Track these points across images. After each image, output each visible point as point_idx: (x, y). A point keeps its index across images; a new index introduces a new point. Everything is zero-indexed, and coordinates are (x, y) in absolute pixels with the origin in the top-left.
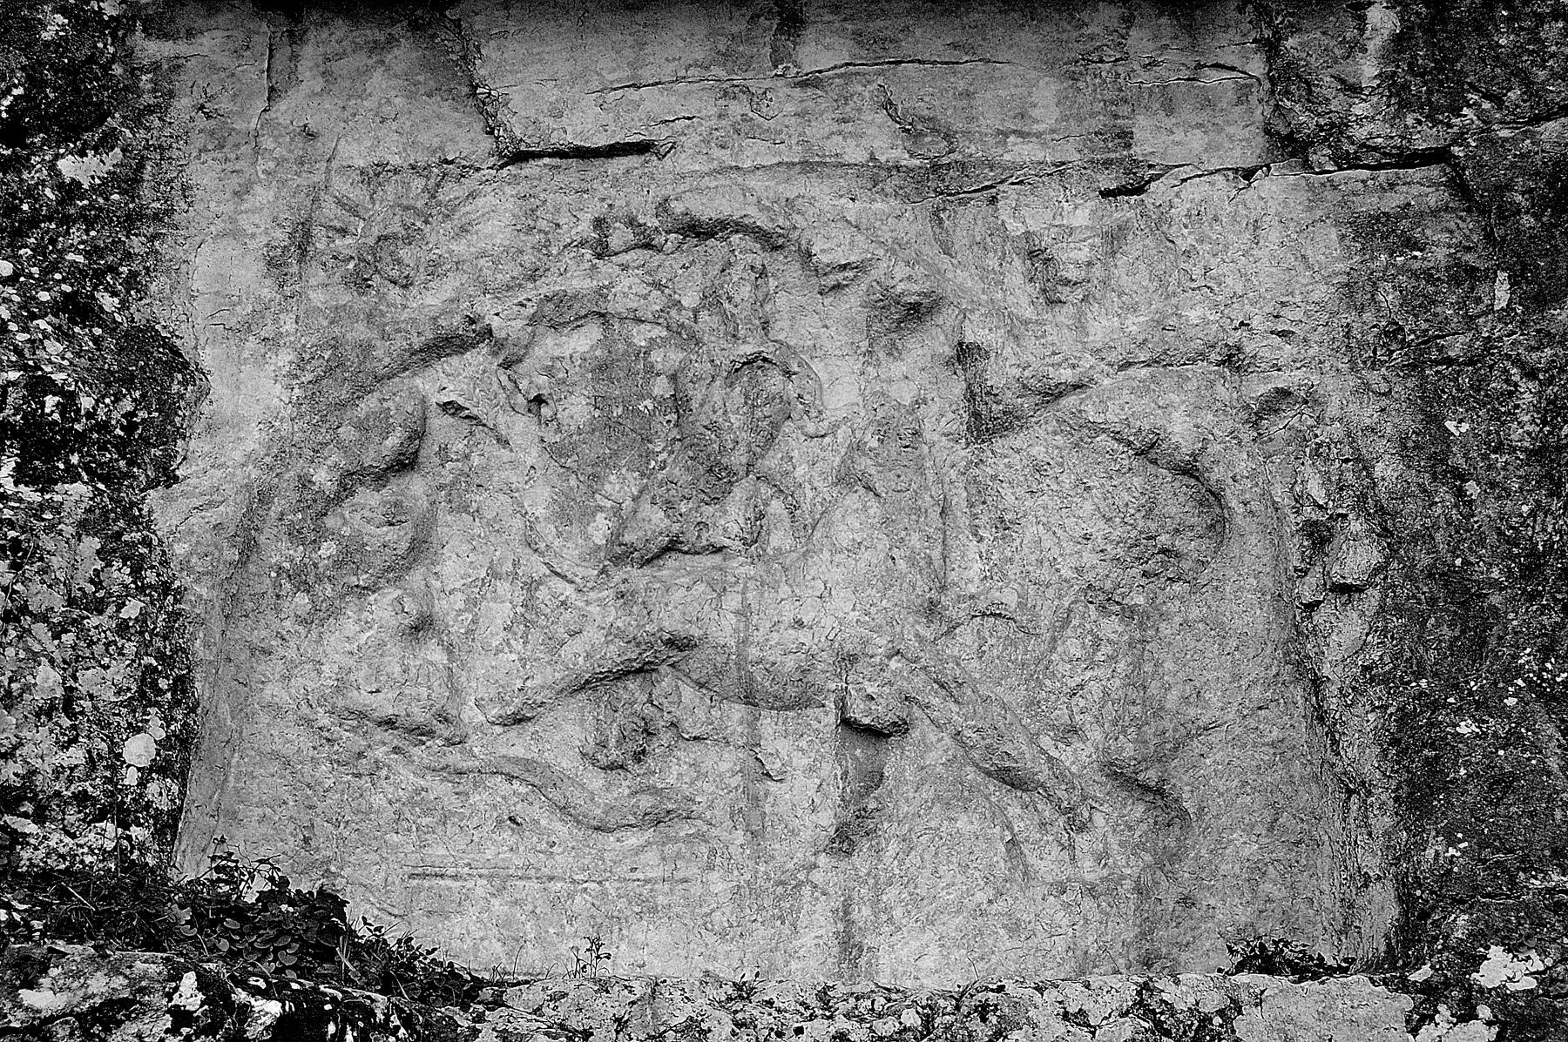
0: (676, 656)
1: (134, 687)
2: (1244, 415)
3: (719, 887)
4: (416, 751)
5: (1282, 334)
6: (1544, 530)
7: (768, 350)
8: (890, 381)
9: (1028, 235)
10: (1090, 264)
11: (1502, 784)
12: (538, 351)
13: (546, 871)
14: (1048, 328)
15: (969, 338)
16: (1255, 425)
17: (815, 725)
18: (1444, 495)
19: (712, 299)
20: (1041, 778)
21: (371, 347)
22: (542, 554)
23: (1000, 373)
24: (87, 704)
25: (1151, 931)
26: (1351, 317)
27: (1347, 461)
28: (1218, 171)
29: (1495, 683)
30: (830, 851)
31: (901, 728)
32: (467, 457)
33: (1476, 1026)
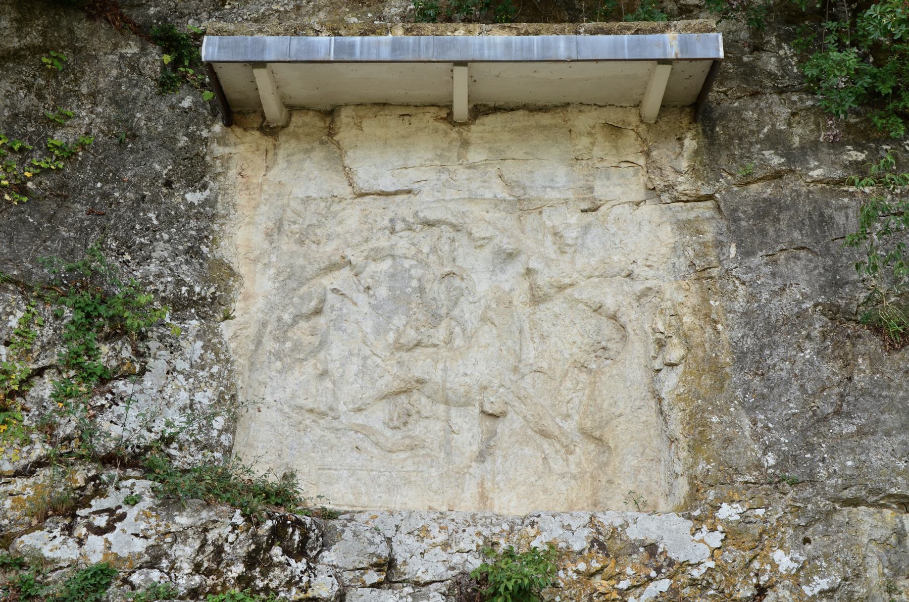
0: (419, 386)
3: (435, 474)
4: (322, 422)
5: (649, 266)
7: (455, 270)
8: (501, 282)
9: (554, 227)
10: (577, 238)
11: (728, 440)
12: (368, 269)
13: (370, 468)
15: (531, 266)
16: (638, 301)
18: (709, 329)
19: (434, 250)
20: (556, 434)
21: (305, 267)
23: (542, 280)
24: (198, 406)
26: (675, 260)
30: (476, 461)
31: (504, 414)
33: (717, 533)
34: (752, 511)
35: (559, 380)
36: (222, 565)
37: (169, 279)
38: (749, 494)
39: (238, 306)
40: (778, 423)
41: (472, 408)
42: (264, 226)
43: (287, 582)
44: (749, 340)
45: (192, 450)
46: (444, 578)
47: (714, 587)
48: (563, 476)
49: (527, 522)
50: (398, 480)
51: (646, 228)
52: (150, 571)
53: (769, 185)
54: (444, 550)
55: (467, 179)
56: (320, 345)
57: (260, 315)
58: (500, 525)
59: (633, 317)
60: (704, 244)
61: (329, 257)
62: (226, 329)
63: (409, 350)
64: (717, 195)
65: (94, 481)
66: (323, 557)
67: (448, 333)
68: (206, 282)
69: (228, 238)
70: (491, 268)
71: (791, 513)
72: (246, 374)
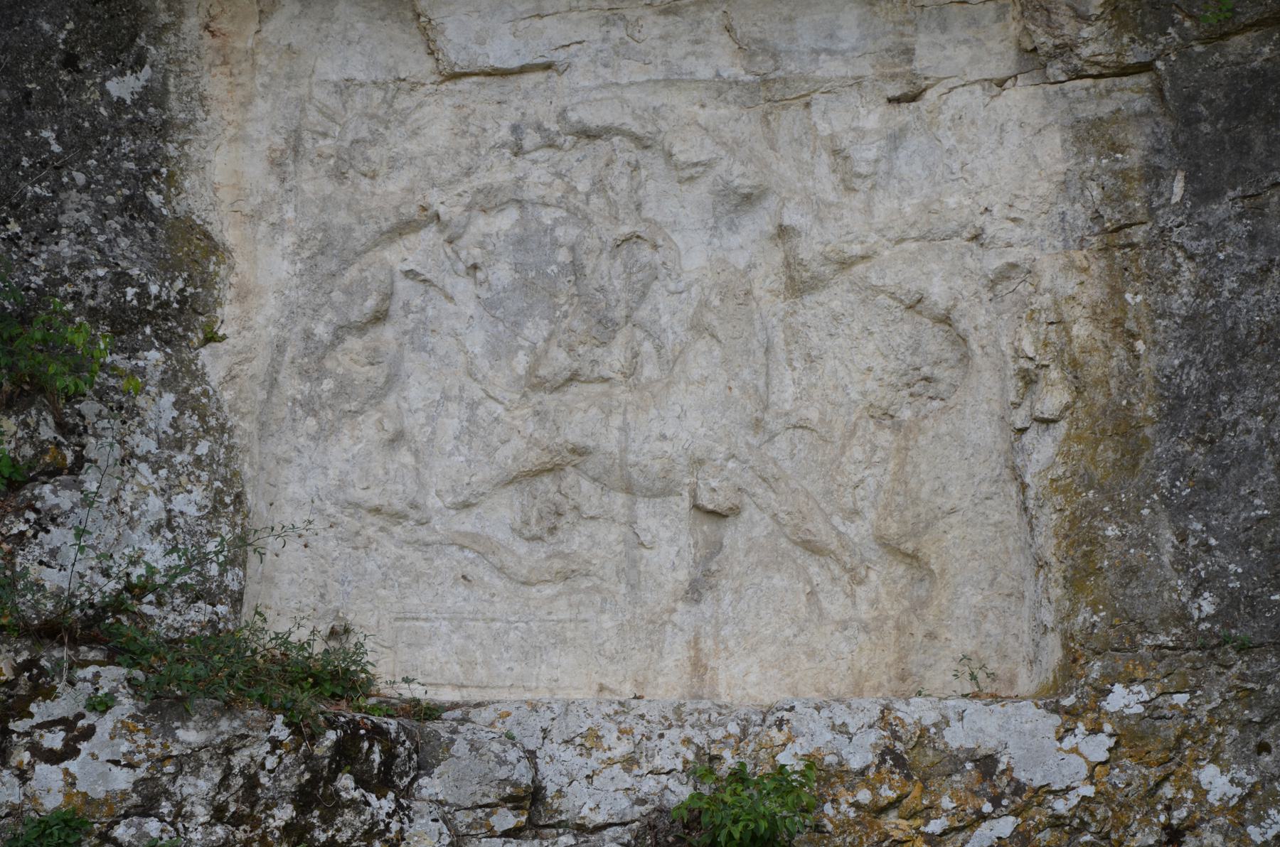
0: (577, 460)
1: (210, 505)
2: (984, 281)
3: (608, 624)
4: (397, 530)
5: (1014, 220)
6: (1188, 379)
7: (641, 229)
8: (730, 250)
9: (832, 137)
10: (877, 161)
11: (1130, 572)
12: (472, 229)
13: (489, 615)
14: (844, 211)
15: (786, 222)
16: (992, 289)
17: (675, 507)
18: (1120, 351)
19: (599, 186)
20: (832, 547)
21: (351, 230)
22: (480, 382)
23: (808, 249)
24: (181, 521)
25: (906, 656)
26: (1065, 206)
27: (1052, 323)
28: (976, 82)
29: (1138, 496)
30: (684, 599)
31: (735, 511)
32: (423, 309)
33: (1101, 737)
34: (1167, 697)
35: (839, 443)
36: (259, 808)
37: (101, 272)
38: (1162, 668)
39: (228, 313)
40: (1228, 535)
41: (677, 499)
42: (267, 144)
43: (366, 833)
44: (1193, 371)
45: (177, 602)
46: (628, 818)
47: (1093, 829)
48: (844, 625)
49: (771, 719)
50: (542, 637)
51: (1013, 138)
52: (143, 820)
53: (1268, 38)
54: (628, 770)
55: (661, 38)
56: (387, 382)
57: (273, 331)
58: (724, 725)
59: (982, 320)
60: (1124, 175)
61: (397, 208)
62: (215, 364)
63: (556, 389)
64: (1159, 64)
65: (30, 670)
66: (420, 788)
67: (629, 355)
68: (166, 271)
69: (196, 171)
70: (711, 222)
71: (1236, 699)
72: (256, 450)
